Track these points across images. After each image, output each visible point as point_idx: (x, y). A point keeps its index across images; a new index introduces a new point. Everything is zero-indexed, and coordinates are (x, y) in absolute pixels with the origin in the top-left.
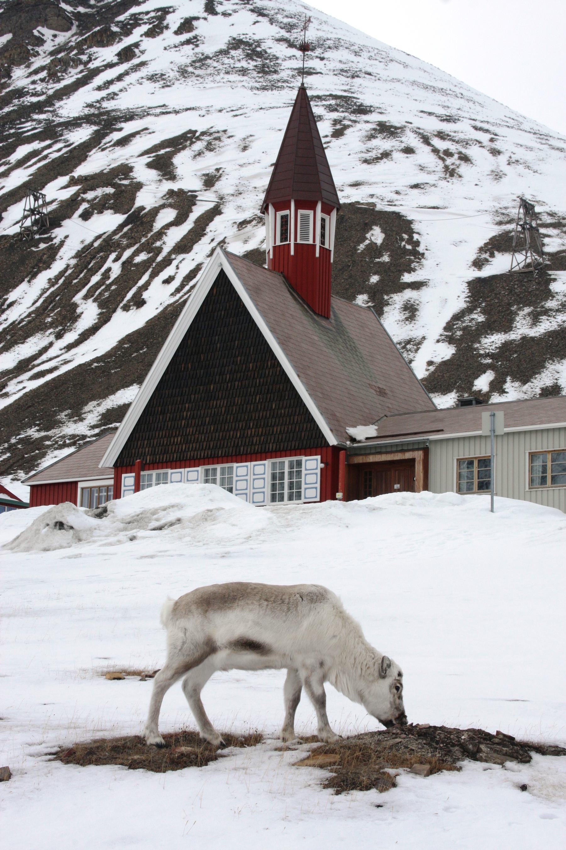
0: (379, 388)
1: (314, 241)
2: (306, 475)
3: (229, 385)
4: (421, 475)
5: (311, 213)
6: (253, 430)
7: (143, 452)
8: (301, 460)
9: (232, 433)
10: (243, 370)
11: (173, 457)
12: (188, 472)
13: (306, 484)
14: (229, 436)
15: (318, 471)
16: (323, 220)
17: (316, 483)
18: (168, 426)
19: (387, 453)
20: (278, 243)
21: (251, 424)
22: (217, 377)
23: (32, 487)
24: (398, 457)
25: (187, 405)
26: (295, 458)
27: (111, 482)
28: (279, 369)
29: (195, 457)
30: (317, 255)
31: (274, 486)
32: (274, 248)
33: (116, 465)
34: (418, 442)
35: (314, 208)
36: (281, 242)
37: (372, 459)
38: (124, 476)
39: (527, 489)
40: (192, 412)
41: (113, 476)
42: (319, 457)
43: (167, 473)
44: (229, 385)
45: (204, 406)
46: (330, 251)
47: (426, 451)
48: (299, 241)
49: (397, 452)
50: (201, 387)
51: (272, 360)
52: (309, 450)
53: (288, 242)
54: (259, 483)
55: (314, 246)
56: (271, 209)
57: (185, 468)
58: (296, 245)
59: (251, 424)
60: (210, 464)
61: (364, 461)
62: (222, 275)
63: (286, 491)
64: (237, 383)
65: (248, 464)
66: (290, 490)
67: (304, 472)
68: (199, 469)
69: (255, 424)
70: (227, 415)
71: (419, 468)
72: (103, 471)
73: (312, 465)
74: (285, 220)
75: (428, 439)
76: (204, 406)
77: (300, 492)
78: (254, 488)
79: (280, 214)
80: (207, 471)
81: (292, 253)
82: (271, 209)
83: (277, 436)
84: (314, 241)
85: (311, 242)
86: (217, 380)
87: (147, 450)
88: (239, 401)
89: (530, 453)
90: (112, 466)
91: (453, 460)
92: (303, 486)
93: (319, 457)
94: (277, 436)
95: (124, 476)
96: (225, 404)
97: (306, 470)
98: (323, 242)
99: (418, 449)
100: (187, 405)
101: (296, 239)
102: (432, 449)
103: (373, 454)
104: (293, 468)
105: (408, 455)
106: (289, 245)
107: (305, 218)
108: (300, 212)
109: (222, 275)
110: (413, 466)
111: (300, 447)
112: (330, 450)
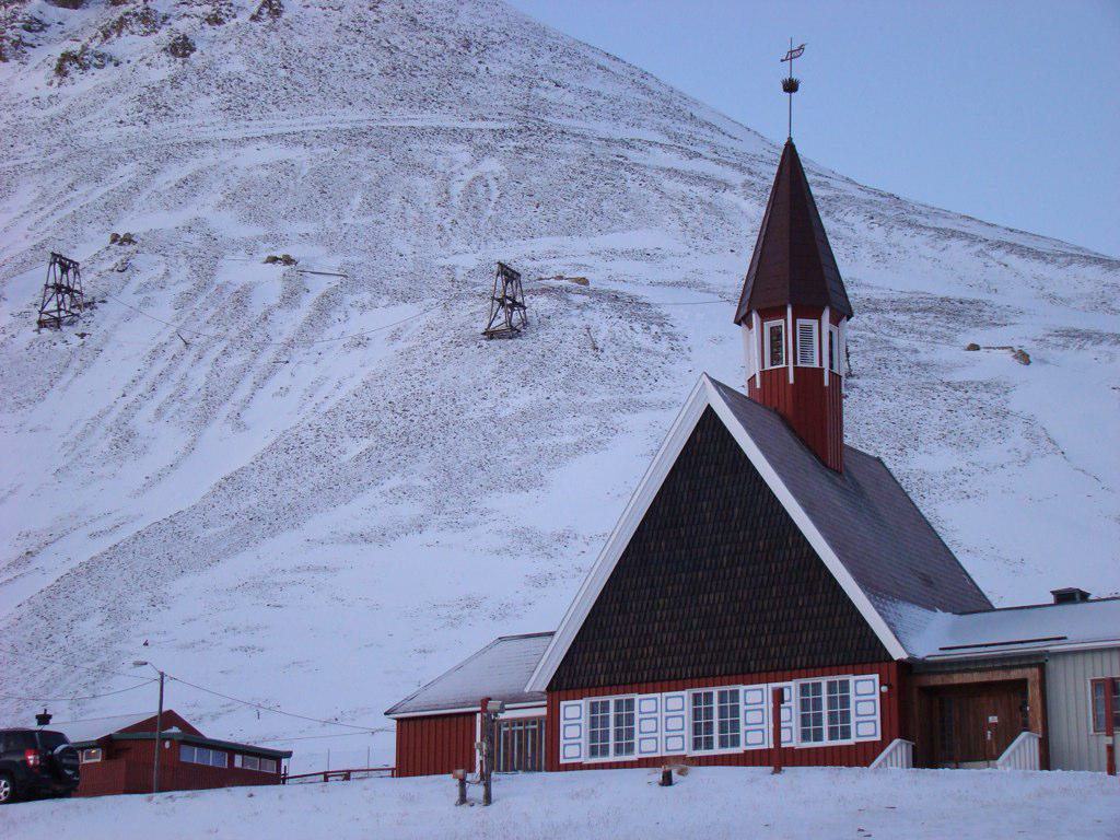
0: (922, 574)
1: (821, 364)
2: (641, 720)
3: (728, 571)
4: (1038, 702)
5: (814, 323)
6: (769, 638)
7: (594, 668)
8: (633, 700)
9: (735, 641)
10: (749, 550)
11: (796, 662)
12: (667, 698)
13: (857, 715)
14: (731, 646)
15: (877, 697)
16: (831, 333)
17: (874, 714)
18: (631, 632)
19: (980, 670)
20: (768, 367)
21: (766, 629)
22: (708, 561)
23: (400, 720)
24: (999, 676)
25: (661, 601)
26: (624, 697)
27: (543, 712)
28: (806, 549)
29: (678, 677)
30: (826, 383)
31: (593, 736)
32: (763, 373)
33: (550, 688)
34: (1029, 656)
35: (818, 317)
36: (772, 365)
37: (957, 679)
38: (562, 703)
39: (1092, 732)
40: (670, 611)
41: (545, 703)
42: (876, 677)
43: (737, 691)
44: (728, 571)
45: (689, 602)
46: (840, 377)
47: (1042, 668)
48: (799, 365)
49: (994, 669)
50: (683, 576)
51: (794, 536)
52: (703, 680)
53: (784, 365)
54: (675, 724)
55: (821, 371)
56: (755, 317)
57: (661, 691)
58: (796, 369)
59: (766, 629)
60: (702, 686)
61: (945, 683)
62: (709, 413)
63: (716, 735)
64: (739, 569)
65: (657, 695)
66: (696, 734)
67: (637, 716)
68: (685, 693)
69: (772, 628)
70: (726, 615)
71: (1033, 693)
72: (531, 697)
73: (865, 690)
74: (776, 334)
75: (1047, 651)
76: (689, 602)
77: (738, 736)
78: (667, 730)
79: (768, 325)
80: (696, 697)
81: (791, 381)
82: (755, 317)
83: (808, 646)
84: (821, 364)
85: (816, 365)
86: (708, 565)
87: (599, 665)
88: (745, 595)
89: (1092, 681)
90: (544, 689)
91: (1085, 683)
92: (742, 727)
93: (876, 677)
94: (808, 646)
95: (562, 703)
96: (722, 600)
97: (641, 712)
98: (831, 366)
99: (1031, 666)
100: (661, 601)
101: (795, 362)
102: (1051, 664)
103: (959, 671)
104: (841, 697)
105: (1015, 674)
106: (786, 369)
107: (807, 331)
108: (800, 322)
109: (709, 413)
110: (1024, 694)
111: (846, 662)
112: (893, 668)
